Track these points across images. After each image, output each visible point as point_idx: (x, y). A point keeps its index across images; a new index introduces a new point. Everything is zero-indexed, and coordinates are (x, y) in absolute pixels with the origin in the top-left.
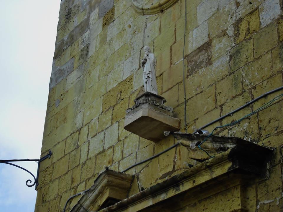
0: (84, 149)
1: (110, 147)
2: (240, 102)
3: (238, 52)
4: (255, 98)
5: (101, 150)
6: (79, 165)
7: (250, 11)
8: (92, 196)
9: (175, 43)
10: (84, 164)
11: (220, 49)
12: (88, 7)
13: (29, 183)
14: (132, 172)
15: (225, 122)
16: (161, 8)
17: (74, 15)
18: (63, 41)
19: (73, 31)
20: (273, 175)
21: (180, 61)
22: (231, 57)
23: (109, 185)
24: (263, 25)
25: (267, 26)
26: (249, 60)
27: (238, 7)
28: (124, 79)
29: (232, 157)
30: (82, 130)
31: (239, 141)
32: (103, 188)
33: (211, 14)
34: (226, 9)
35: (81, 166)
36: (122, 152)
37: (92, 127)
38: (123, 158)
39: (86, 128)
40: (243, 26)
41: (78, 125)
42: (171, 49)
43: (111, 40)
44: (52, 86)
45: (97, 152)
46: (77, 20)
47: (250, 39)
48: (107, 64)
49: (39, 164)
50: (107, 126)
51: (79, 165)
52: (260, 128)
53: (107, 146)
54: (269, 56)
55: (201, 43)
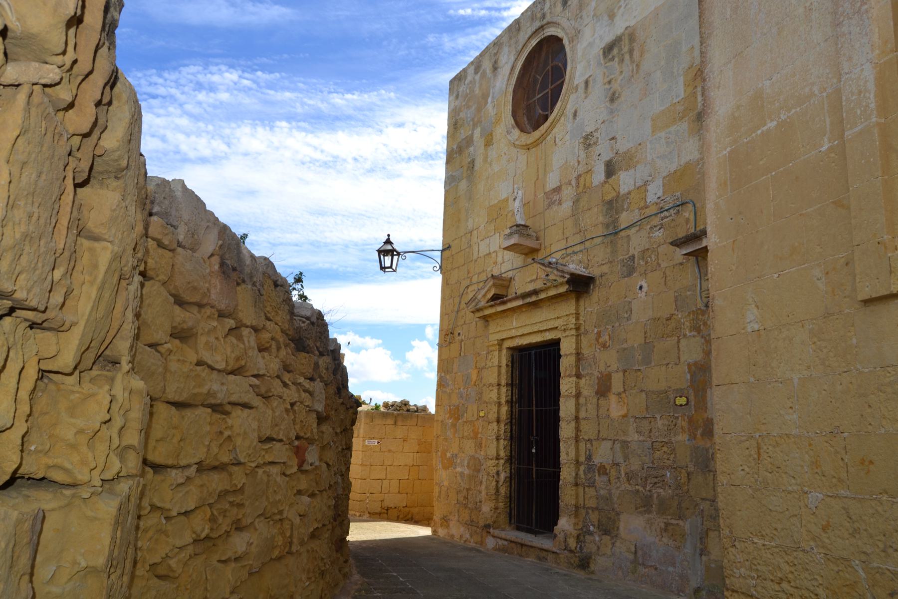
0: (475, 248)
1: (494, 252)
2: (578, 239)
3: (578, 200)
4: (587, 238)
5: (488, 252)
6: (472, 261)
7: (586, 171)
8: (483, 292)
9: (537, 179)
10: (476, 261)
11: (567, 194)
12: (471, 123)
13: (435, 269)
14: (510, 274)
15: (569, 251)
16: (528, 147)
17: (460, 127)
18: (453, 149)
19: (460, 142)
20: (594, 293)
21: (541, 195)
22: (573, 202)
23: (494, 285)
24: (594, 185)
25: (596, 186)
26: (585, 209)
27: (579, 164)
28: (503, 198)
29: (568, 282)
30: (473, 233)
31: (572, 274)
32: (490, 287)
33: (562, 164)
34: (572, 164)
35: (473, 262)
36: (503, 257)
37: (480, 233)
38: (503, 262)
39: (475, 232)
40: (582, 180)
41: (469, 228)
42: (535, 184)
43: (491, 161)
44: (447, 188)
45: (485, 253)
46: (463, 134)
47: (585, 192)
48: (489, 181)
49: (441, 253)
50: (492, 234)
51: (472, 261)
52: (588, 260)
53: (492, 251)
54: (596, 209)
55: (555, 186)
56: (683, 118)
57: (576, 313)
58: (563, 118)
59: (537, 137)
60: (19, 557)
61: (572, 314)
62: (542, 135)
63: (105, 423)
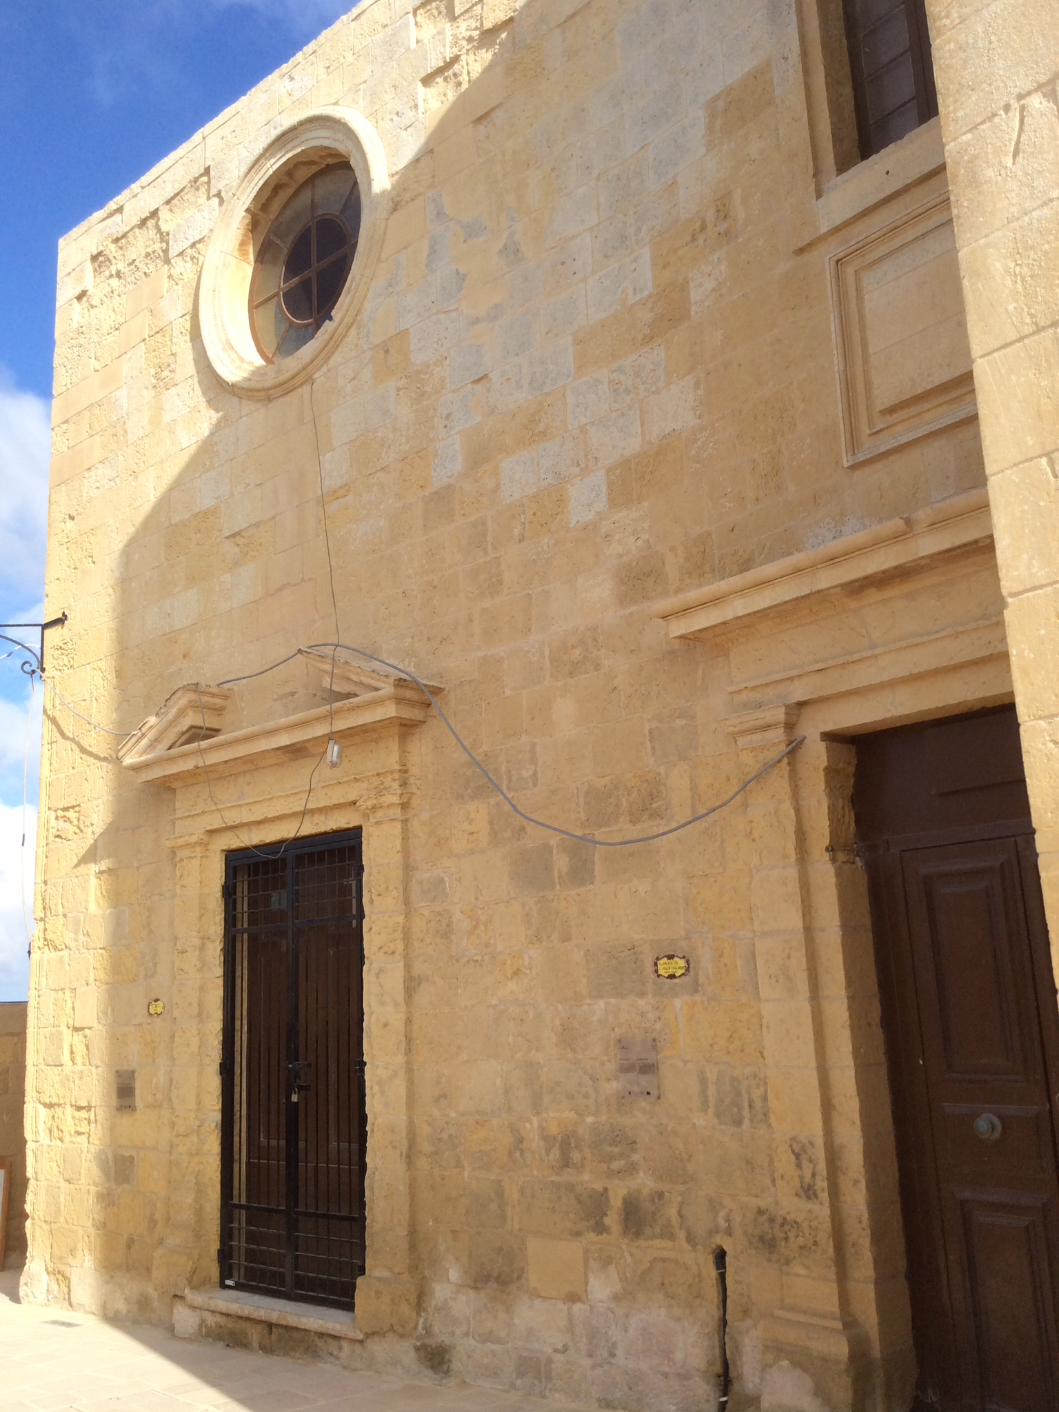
34: (379, 434)
56: (652, 338)
57: (400, 771)
58: (353, 332)
59: (307, 359)
60: (324, 479)
61: (392, 772)
62: (304, 368)
63: (744, 402)
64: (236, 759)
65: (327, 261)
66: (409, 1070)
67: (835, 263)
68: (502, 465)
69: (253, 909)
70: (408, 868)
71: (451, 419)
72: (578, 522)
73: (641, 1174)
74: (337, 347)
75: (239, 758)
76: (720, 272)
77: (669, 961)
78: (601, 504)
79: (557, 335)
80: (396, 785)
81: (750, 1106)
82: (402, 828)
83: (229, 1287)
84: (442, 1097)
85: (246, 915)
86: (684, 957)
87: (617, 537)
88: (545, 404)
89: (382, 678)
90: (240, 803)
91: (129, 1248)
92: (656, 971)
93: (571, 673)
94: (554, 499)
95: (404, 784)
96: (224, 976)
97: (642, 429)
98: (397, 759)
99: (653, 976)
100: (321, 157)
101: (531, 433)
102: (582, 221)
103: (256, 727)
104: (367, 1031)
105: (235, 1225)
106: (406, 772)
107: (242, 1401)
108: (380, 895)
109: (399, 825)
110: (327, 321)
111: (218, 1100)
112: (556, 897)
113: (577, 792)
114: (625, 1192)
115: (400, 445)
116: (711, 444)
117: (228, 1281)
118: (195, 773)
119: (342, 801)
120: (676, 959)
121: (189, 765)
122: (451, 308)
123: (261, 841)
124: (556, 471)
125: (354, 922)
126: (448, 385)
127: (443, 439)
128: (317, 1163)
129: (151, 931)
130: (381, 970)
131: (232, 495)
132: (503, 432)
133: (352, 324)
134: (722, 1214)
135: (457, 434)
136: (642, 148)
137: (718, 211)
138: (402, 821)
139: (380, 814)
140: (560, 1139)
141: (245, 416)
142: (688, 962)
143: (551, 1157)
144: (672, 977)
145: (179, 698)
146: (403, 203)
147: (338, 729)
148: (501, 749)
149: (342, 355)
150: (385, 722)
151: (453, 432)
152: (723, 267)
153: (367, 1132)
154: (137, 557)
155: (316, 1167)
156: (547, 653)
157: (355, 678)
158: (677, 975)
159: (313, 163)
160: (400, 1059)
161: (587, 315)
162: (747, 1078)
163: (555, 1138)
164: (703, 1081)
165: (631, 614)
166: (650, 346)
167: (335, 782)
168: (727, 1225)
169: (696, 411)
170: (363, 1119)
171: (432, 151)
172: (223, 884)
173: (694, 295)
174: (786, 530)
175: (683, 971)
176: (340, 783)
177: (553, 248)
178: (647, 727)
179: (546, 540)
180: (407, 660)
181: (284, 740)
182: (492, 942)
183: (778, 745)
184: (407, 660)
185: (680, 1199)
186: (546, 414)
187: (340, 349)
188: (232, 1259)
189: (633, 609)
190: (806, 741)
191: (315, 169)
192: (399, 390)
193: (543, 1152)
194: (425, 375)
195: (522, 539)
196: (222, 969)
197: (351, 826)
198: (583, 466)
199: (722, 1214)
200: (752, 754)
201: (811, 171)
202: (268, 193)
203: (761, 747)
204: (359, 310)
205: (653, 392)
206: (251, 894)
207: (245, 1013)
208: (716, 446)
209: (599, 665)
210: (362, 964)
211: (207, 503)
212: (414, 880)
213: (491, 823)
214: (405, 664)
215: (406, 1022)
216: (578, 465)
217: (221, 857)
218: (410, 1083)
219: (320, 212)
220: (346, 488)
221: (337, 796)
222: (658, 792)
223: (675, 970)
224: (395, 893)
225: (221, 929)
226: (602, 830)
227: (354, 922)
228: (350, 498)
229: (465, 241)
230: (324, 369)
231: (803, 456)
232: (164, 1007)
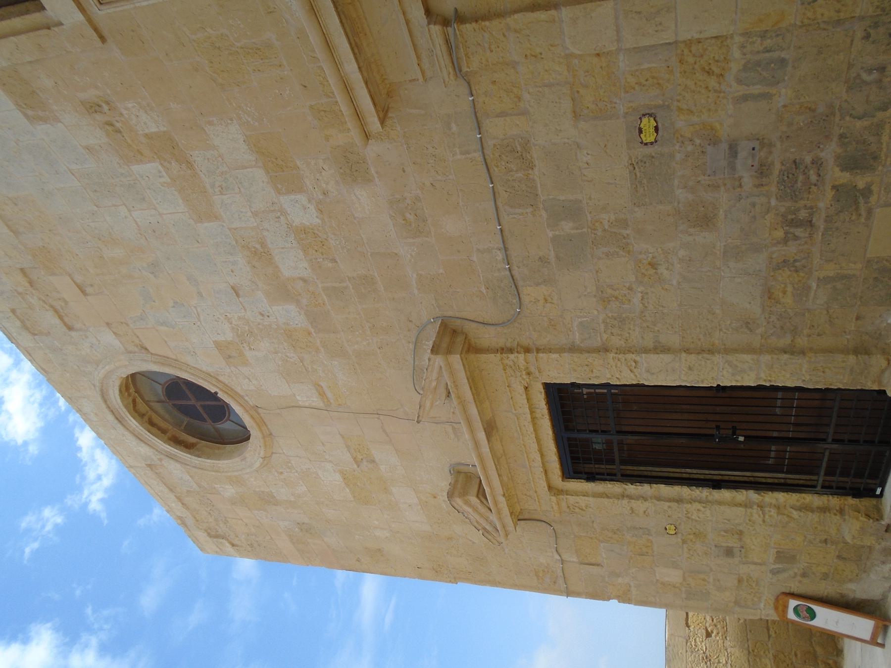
58: (221, 378)
64: (497, 469)
65: (190, 395)
66: (727, 351)
67: (102, 6)
68: (287, 275)
69: (603, 461)
70: (573, 349)
71: (263, 313)
72: (317, 217)
73: (822, 155)
74: (232, 389)
75: (496, 467)
76: (133, 107)
77: (643, 132)
78: (302, 198)
79: (199, 235)
80: (512, 356)
81: (768, 51)
82: (543, 353)
83: (882, 492)
84: (748, 325)
85: (608, 467)
86: (640, 118)
87: (324, 186)
88: (243, 244)
89: (431, 363)
90: (528, 467)
91: (844, 559)
92: (652, 143)
93: (424, 221)
94: (304, 235)
95: (511, 351)
96: (650, 483)
97: (248, 168)
98: (493, 355)
99: (656, 147)
100: (129, 395)
101: (263, 254)
102: (126, 217)
103: (681, 441)
104: (694, 383)
105: (834, 485)
106: (503, 349)
107: (890, 470)
108: (592, 371)
109: (541, 355)
110: (218, 395)
111: (739, 491)
112: (593, 231)
113: (511, 214)
114: (837, 169)
115: (285, 349)
116: (249, 109)
117: (877, 492)
118: (508, 496)
119: (524, 396)
120: (642, 126)
121: (502, 500)
122: (195, 311)
123: (555, 454)
124: (285, 235)
125: (613, 391)
126: (243, 314)
127: (276, 318)
128: (791, 423)
129: (618, 530)
130: (648, 371)
131: (330, 461)
132: (266, 275)
133: (217, 379)
134: (865, 76)
135: (272, 309)
136: (73, 174)
137: (96, 112)
138: (537, 353)
139: (532, 369)
140: (787, 228)
141: (283, 451)
142: (644, 115)
143: (802, 235)
144: (656, 129)
145: (457, 504)
146: (141, 343)
147: (472, 397)
148: (483, 276)
149: (236, 386)
150: (465, 362)
151: (271, 311)
152: (130, 105)
153: (771, 385)
154: (376, 523)
155: (795, 424)
156: (411, 240)
157: (434, 384)
158: (655, 124)
159: (134, 401)
160: (717, 358)
161: (182, 212)
162: (744, 54)
163: (786, 233)
164: (745, 98)
165: (377, 173)
166: (193, 163)
167: (511, 401)
168: (875, 71)
169: (228, 123)
170: (760, 388)
171: (108, 324)
172: (585, 481)
173: (154, 129)
174: (298, 38)
175: (652, 119)
176: (512, 398)
177: (146, 239)
178: (459, 157)
179: (333, 242)
180: (424, 347)
181: (482, 436)
182: (627, 285)
183: (462, 31)
184: (424, 347)
185: (848, 118)
186: (249, 243)
187: (233, 387)
188: (860, 489)
189: (373, 170)
190: (457, 8)
191: (139, 400)
192: (250, 349)
193: (798, 242)
194: (239, 330)
195: (334, 261)
196: (645, 484)
197: (543, 391)
198: (279, 214)
199: (865, 76)
200: (471, 57)
201: (46, 31)
202: (154, 430)
203: (464, 47)
204: (207, 374)
205: (223, 160)
206: (593, 462)
207: (678, 470)
208: (249, 105)
209: (416, 198)
210: (643, 385)
211: (338, 477)
212: (582, 345)
213: (537, 284)
214: (428, 349)
215: (688, 353)
216: (279, 217)
217: (568, 482)
218: (735, 351)
219: (163, 398)
220: (318, 388)
221: (522, 399)
222: (508, 146)
223: (651, 127)
224: (590, 360)
225: (617, 484)
226: (540, 194)
227: (613, 391)
228: (323, 384)
229: (154, 301)
230: (246, 398)
231: (242, 26)
232: (671, 524)
